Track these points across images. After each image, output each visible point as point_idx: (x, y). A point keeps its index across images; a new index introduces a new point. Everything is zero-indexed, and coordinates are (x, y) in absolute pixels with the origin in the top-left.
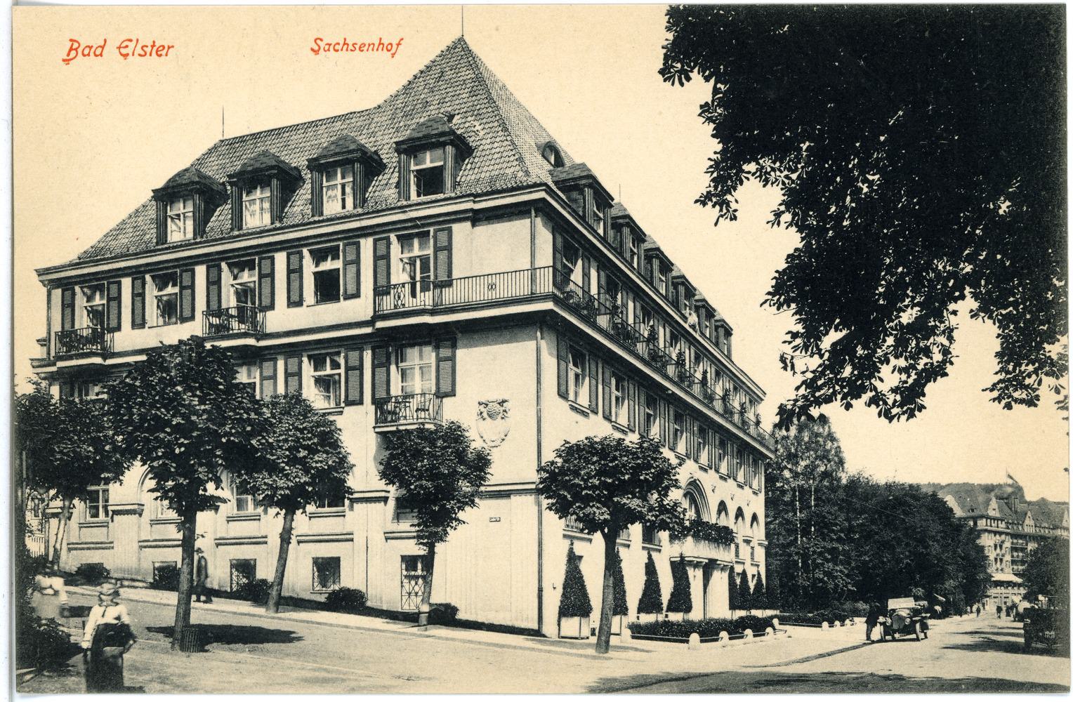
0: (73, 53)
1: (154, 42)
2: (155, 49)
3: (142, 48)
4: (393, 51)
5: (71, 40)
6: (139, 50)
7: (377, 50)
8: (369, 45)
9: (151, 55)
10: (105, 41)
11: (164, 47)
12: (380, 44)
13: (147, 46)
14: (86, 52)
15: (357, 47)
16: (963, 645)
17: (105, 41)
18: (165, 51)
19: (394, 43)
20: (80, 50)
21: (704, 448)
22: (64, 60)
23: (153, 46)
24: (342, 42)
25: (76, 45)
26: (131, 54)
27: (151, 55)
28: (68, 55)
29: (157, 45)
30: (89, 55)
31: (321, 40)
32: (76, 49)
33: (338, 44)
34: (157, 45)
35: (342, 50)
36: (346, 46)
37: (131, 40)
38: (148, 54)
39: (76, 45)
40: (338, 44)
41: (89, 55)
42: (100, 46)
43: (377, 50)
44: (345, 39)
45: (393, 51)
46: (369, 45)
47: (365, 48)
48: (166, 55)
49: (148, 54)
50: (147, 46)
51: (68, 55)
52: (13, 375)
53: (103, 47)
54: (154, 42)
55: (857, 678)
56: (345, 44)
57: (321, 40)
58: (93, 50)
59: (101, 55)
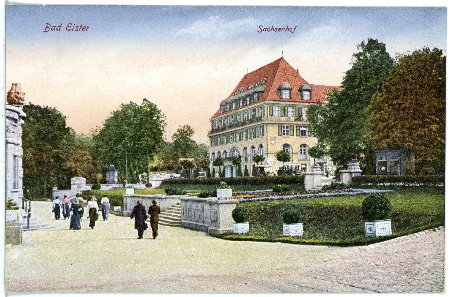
0: (47, 29)
1: (81, 25)
2: (82, 28)
3: (76, 27)
4: (292, 31)
5: (47, 24)
6: (75, 28)
7: (286, 31)
8: (283, 29)
9: (80, 30)
10: (61, 24)
11: (85, 27)
12: (287, 28)
13: (78, 27)
14: (53, 28)
15: (277, 30)
16: (7, 186)
17: (61, 24)
18: (86, 28)
19: (293, 28)
20: (50, 28)
21: (246, 118)
22: (44, 32)
23: (81, 27)
24: (271, 28)
25: (49, 26)
26: (71, 30)
27: (80, 30)
28: (45, 30)
29: (83, 26)
30: (54, 30)
31: (262, 26)
32: (49, 27)
33: (269, 28)
34: (83, 26)
35: (271, 31)
36: (273, 29)
37: (72, 24)
38: (79, 30)
39: (49, 26)
40: (269, 28)
41: (54, 30)
42: (59, 27)
43: (286, 31)
44: (272, 26)
45: (292, 31)
46: (283, 29)
47: (85, 29)
48: (87, 30)
49: (79, 30)
50: (78, 27)
51: (45, 30)
52: (6, 182)
53: (60, 27)
54: (81, 25)
55: (190, 173)
56: (272, 28)
57: (262, 26)
58: (56, 28)
59: (59, 30)
